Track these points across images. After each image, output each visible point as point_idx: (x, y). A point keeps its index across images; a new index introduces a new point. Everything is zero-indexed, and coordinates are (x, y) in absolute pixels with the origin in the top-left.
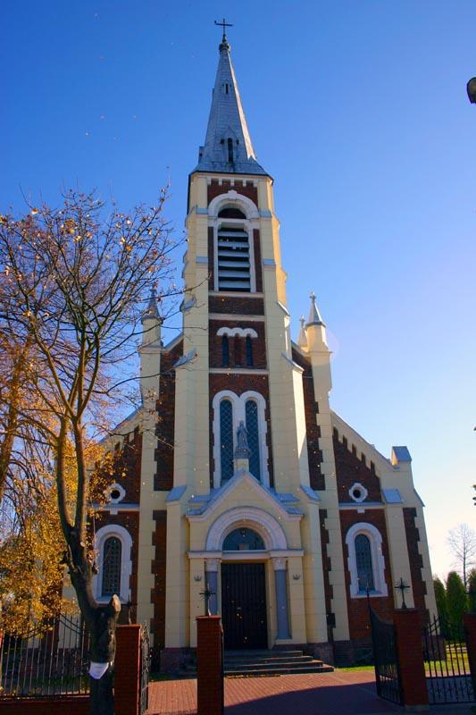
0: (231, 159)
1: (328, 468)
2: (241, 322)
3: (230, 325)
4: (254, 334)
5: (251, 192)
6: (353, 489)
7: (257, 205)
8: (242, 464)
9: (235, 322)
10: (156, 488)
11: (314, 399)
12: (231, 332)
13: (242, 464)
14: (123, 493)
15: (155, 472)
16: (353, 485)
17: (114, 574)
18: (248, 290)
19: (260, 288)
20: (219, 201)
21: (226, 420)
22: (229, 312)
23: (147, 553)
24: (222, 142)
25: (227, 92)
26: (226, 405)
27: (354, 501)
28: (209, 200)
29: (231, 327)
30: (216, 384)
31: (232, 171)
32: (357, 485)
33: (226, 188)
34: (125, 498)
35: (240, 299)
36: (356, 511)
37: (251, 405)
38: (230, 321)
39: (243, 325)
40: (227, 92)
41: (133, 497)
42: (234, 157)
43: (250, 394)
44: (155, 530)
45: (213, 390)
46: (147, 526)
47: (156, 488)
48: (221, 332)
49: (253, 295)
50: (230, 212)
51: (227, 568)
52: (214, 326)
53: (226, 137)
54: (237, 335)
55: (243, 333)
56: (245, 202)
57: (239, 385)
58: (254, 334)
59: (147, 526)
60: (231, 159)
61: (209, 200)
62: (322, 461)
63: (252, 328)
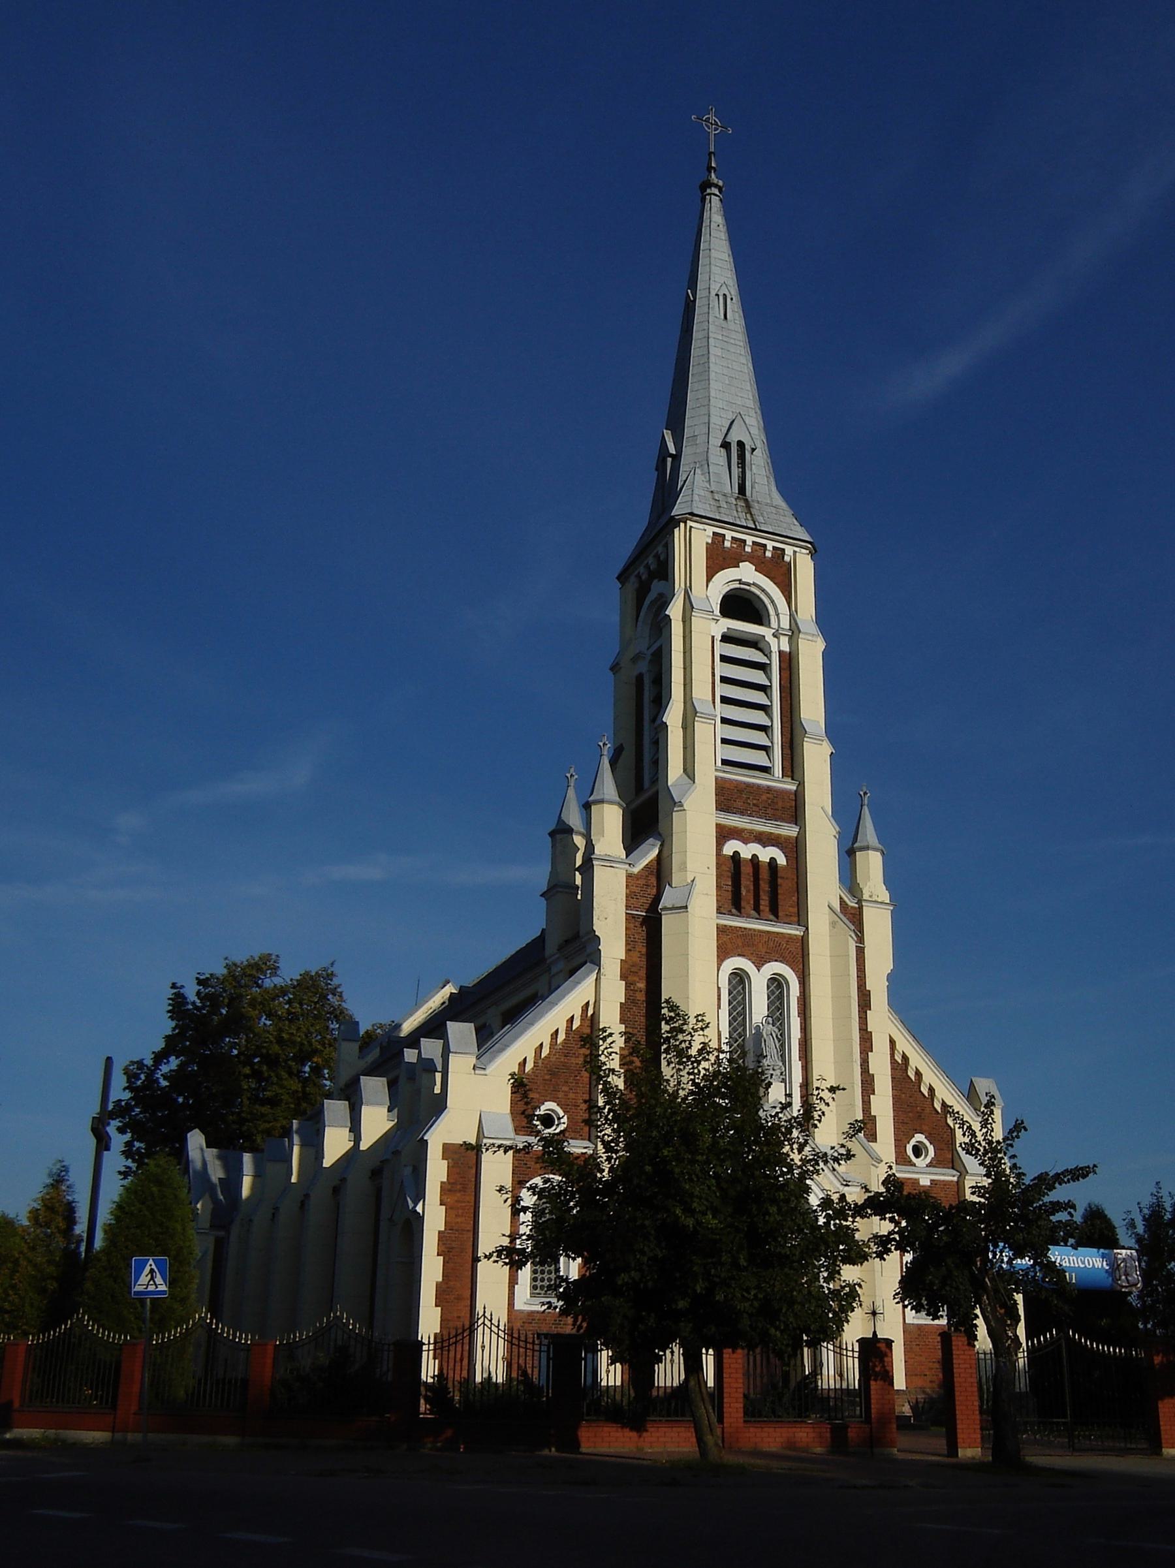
1: (883, 1106)
2: (761, 833)
9: (751, 832)
10: (444, 1145)
12: (747, 851)
17: (539, 1283)
18: (765, 770)
20: (725, 581)
22: (742, 813)
25: (725, 317)
26: (739, 979)
27: (914, 1165)
29: (746, 841)
32: (919, 1137)
35: (759, 786)
36: (916, 1181)
37: (777, 985)
38: (743, 830)
39: (765, 840)
40: (725, 317)
43: (776, 967)
44: (440, 1279)
47: (444, 1145)
49: (777, 781)
55: (766, 854)
57: (761, 950)
60: (742, 489)
62: (440, 1232)
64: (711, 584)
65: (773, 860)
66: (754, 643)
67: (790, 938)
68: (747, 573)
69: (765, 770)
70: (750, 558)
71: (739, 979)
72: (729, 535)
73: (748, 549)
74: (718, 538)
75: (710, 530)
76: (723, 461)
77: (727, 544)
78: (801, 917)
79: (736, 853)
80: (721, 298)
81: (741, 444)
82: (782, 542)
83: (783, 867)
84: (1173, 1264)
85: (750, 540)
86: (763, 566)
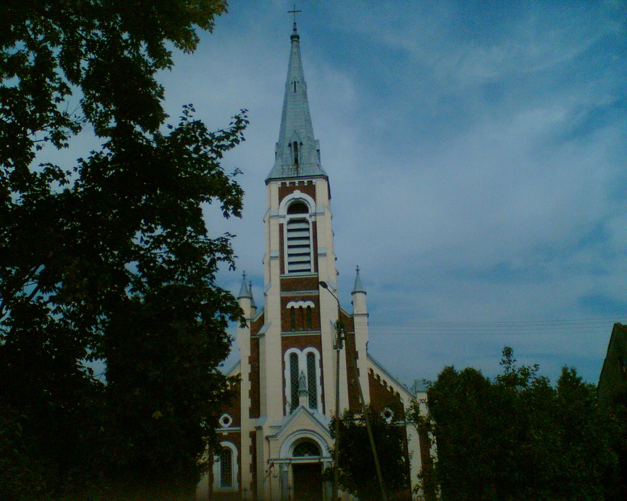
0: (296, 161)
3: (295, 299)
4: (312, 305)
5: (311, 190)
6: (229, 417)
7: (315, 202)
8: (304, 400)
10: (250, 418)
11: (355, 349)
12: (296, 305)
13: (304, 400)
14: (231, 420)
15: (250, 406)
16: (231, 417)
18: (309, 270)
19: (316, 270)
21: (313, 402)
23: (247, 458)
24: (290, 145)
28: (280, 199)
29: (296, 301)
30: (286, 343)
31: (295, 175)
32: (226, 415)
33: (290, 190)
34: (232, 424)
37: (311, 356)
39: (304, 299)
41: (237, 422)
42: (299, 158)
45: (285, 348)
46: (246, 442)
47: (250, 418)
48: (289, 306)
50: (298, 207)
51: (297, 468)
52: (284, 301)
53: (293, 141)
54: (301, 307)
55: (305, 305)
56: (307, 198)
57: (301, 343)
58: (312, 305)
59: (246, 442)
60: (296, 161)
61: (280, 199)
63: (310, 300)
64: (281, 203)
65: (309, 307)
66: (304, 221)
67: (319, 335)
68: (297, 194)
69: (309, 270)
70: (298, 188)
71: (294, 357)
72: (288, 182)
73: (297, 185)
74: (284, 184)
75: (279, 183)
76: (288, 152)
77: (288, 185)
78: (318, 327)
79: (293, 307)
80: (293, 83)
81: (295, 143)
82: (311, 178)
83: (313, 308)
84: (1, 433)
85: (297, 181)
86: (303, 189)
